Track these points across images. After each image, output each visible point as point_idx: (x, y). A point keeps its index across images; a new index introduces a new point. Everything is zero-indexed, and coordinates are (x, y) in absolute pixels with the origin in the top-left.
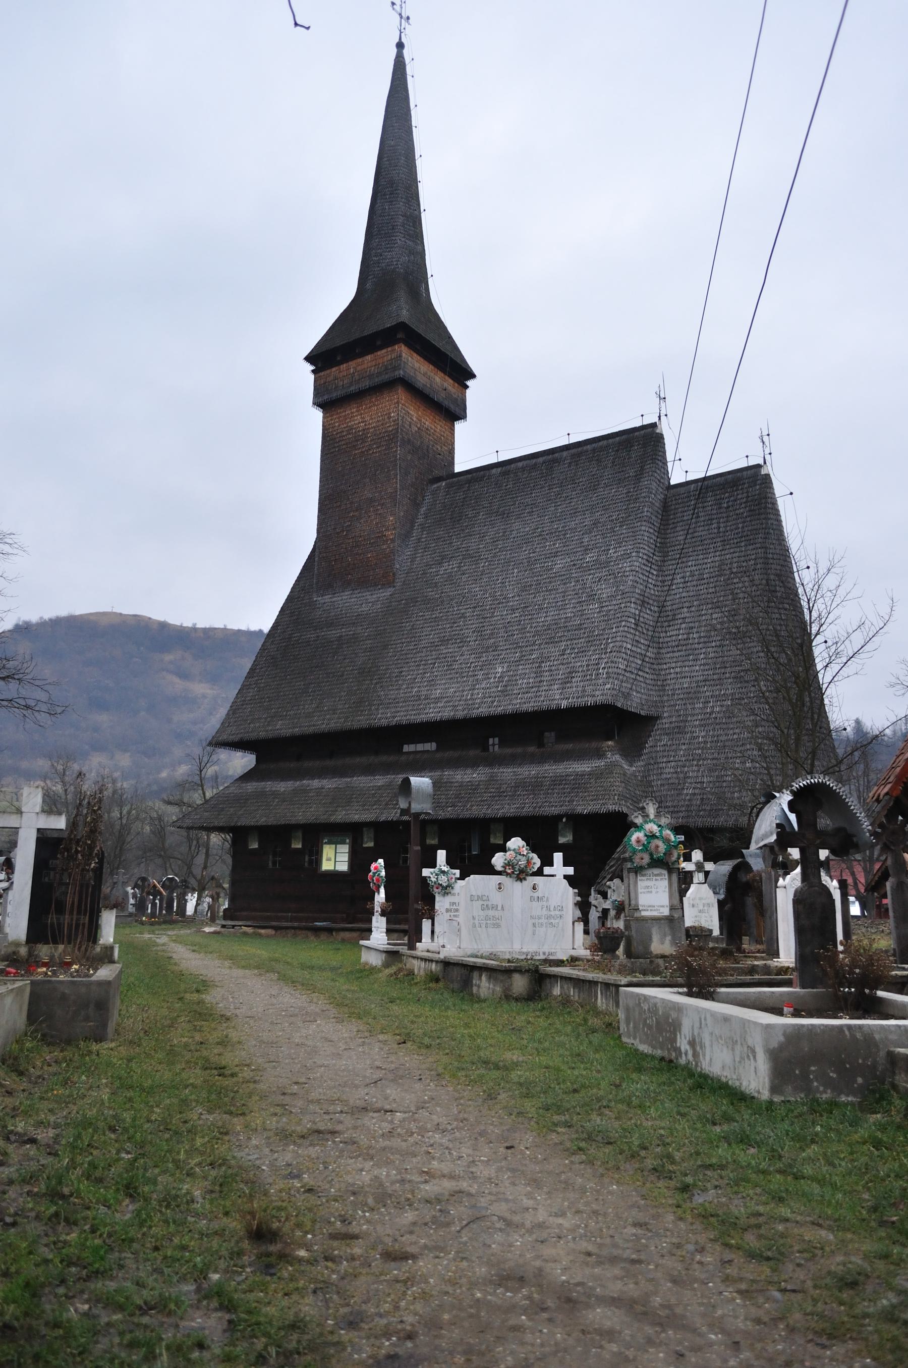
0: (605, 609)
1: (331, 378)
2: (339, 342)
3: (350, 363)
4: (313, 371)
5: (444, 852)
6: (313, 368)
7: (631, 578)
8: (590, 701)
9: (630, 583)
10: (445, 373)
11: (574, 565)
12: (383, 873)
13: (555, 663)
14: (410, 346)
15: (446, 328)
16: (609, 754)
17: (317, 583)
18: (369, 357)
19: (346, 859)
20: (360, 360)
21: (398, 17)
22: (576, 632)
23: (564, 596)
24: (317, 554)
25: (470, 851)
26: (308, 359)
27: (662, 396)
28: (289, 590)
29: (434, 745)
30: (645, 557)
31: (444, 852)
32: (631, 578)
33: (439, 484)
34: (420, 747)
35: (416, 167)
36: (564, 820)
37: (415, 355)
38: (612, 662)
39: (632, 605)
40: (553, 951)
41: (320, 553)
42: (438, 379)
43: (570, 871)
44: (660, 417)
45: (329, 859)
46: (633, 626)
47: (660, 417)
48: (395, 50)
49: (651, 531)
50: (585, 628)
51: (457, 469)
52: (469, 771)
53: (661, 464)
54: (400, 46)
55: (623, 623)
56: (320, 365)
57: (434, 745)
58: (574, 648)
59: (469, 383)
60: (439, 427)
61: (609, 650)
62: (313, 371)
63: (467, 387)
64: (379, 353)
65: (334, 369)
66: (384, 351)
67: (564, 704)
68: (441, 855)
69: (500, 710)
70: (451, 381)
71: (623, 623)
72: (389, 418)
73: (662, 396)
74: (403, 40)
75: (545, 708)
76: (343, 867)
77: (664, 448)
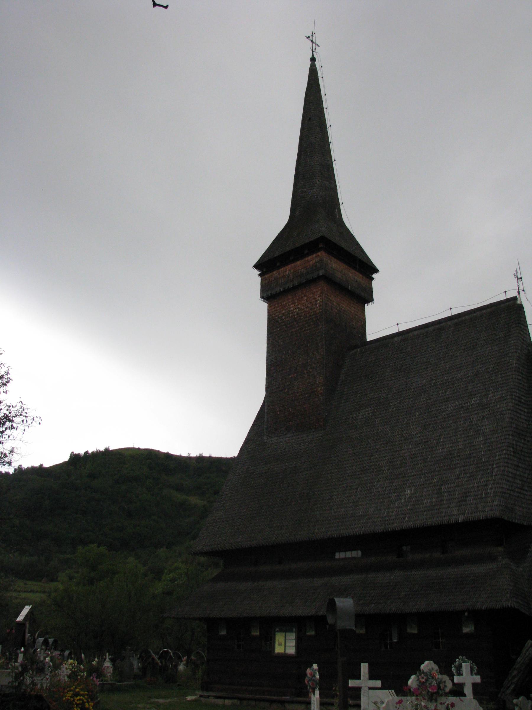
0: (489, 441)
1: (273, 278)
2: (277, 254)
3: (286, 267)
4: (260, 275)
5: (367, 665)
6: (259, 272)
7: (507, 415)
8: (482, 516)
9: (507, 420)
10: (356, 270)
11: (462, 407)
12: (317, 676)
13: (452, 485)
14: (330, 253)
15: (355, 238)
16: (500, 558)
17: (266, 429)
18: (299, 262)
19: (294, 644)
20: (293, 265)
21: (311, 43)
22: (467, 460)
23: (455, 432)
24: (266, 407)
25: (391, 639)
26: (256, 266)
27: (519, 276)
28: (247, 434)
29: (360, 553)
30: (517, 399)
31: (367, 665)
32: (507, 415)
33: (355, 350)
34: (349, 554)
35: (327, 133)
36: (466, 614)
37: (333, 258)
38: (498, 483)
39: (510, 437)
40: (464, 701)
41: (269, 406)
42: (350, 274)
43: (478, 679)
44: (519, 292)
45: (280, 644)
46: (512, 453)
47: (519, 292)
48: (309, 63)
49: (520, 378)
50: (474, 457)
51: (369, 338)
52: (388, 574)
53: (523, 327)
54: (313, 59)
55: (504, 452)
56: (264, 270)
57: (360, 553)
58: (466, 473)
59: (374, 276)
60: (353, 309)
61: (494, 474)
62: (260, 275)
63: (373, 279)
64: (306, 259)
65: (274, 272)
66: (310, 257)
67: (461, 519)
68: (365, 668)
69: (410, 524)
70: (360, 275)
71: (504, 452)
72: (316, 304)
73: (519, 276)
74: (315, 56)
75: (446, 522)
76: (292, 651)
77: (524, 314)
